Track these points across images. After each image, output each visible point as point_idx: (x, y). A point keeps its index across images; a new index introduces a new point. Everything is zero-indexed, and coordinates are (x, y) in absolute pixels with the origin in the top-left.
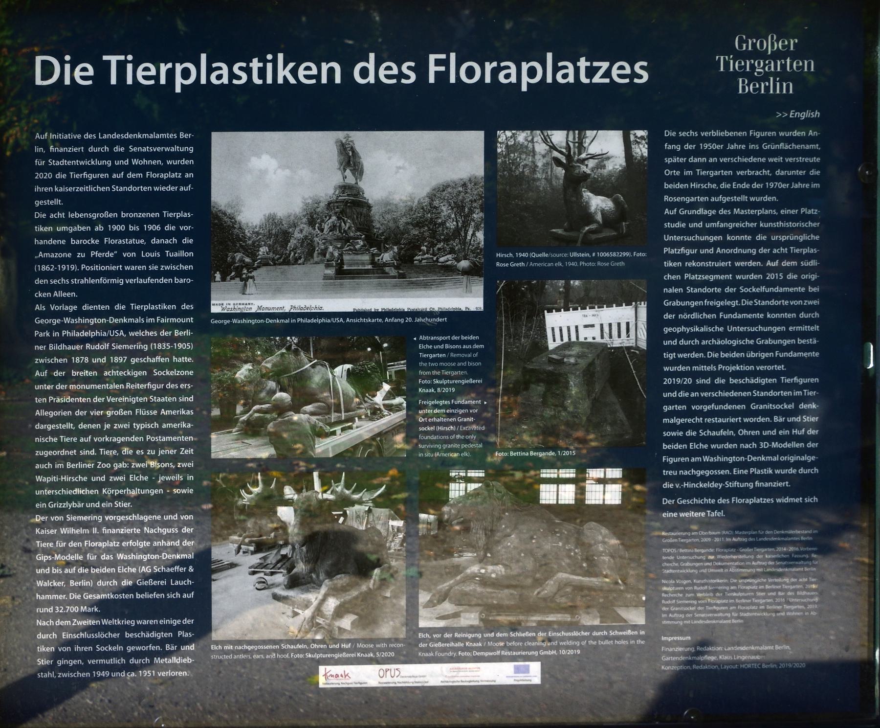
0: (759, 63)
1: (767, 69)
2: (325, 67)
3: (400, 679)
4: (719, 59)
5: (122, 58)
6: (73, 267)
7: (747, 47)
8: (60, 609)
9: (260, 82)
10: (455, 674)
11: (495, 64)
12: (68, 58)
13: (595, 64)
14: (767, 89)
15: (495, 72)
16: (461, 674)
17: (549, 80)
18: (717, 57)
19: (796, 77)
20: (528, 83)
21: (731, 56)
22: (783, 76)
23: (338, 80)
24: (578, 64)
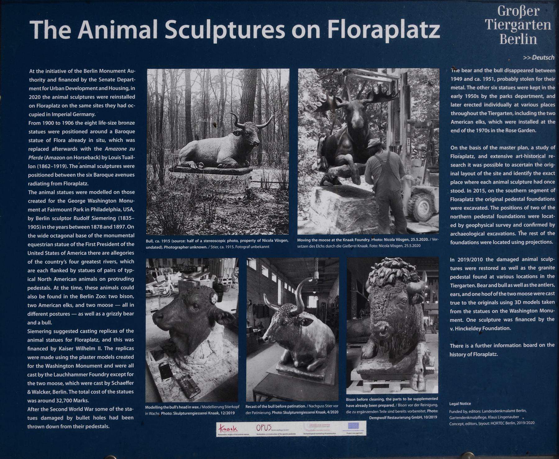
0: (514, 25)
2: (310, 28)
3: (270, 432)
4: (487, 21)
5: (41, 22)
6: (64, 166)
7: (506, 13)
8: (59, 400)
9: (234, 37)
10: (312, 429)
11: (369, 26)
12: (112, 22)
13: (431, 26)
14: (519, 41)
15: (369, 31)
16: (317, 428)
17: (403, 36)
18: (486, 20)
19: (540, 34)
20: (218, 39)
21: (495, 19)
22: (531, 32)
23: (318, 36)
24: (421, 26)
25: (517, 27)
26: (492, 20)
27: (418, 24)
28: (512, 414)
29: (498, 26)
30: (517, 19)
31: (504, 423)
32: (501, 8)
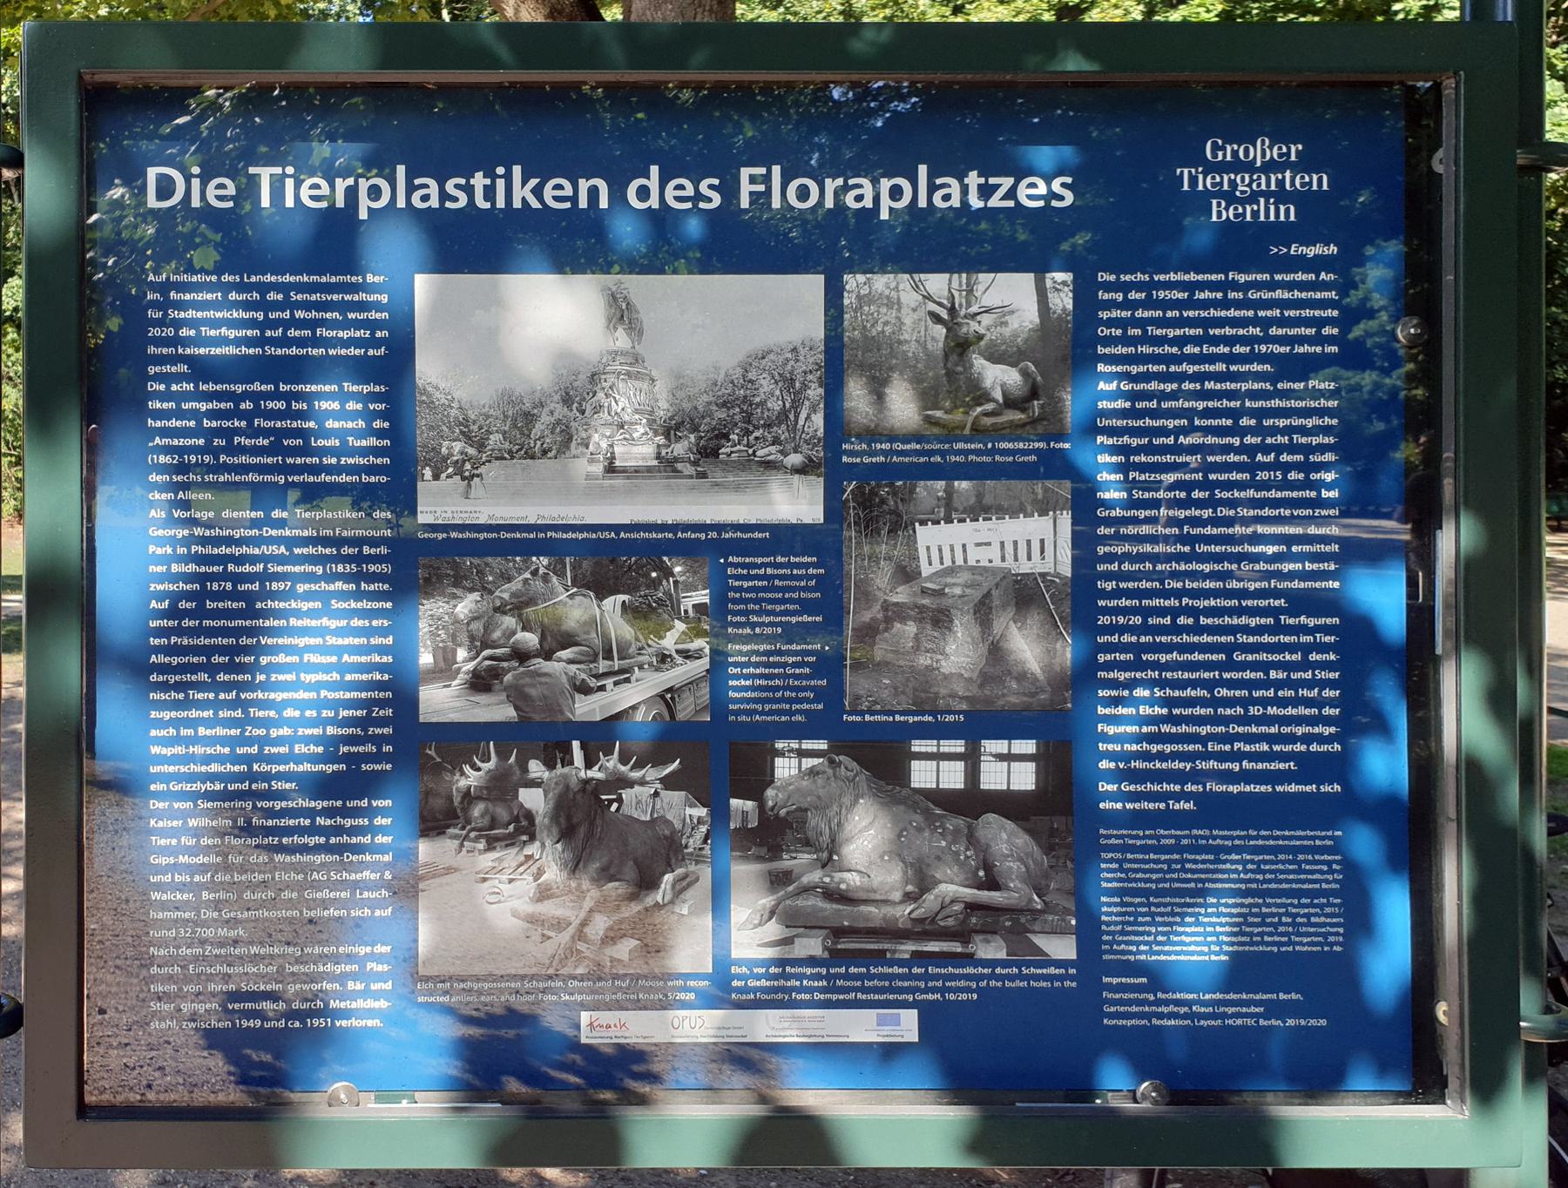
0: (1243, 180)
1: (1254, 186)
2: (584, 185)
4: (1182, 172)
7: (1225, 155)
9: (487, 205)
11: (840, 181)
13: (992, 181)
14: (1255, 214)
15: (840, 193)
18: (1178, 171)
19: (1302, 199)
21: (1200, 169)
22: (1281, 196)
25: (1249, 185)
26: (1193, 170)
27: (960, 177)
28: (1247, 1003)
29: (1206, 182)
30: (1249, 167)
31: (1257, 1022)
32: (1215, 144)
